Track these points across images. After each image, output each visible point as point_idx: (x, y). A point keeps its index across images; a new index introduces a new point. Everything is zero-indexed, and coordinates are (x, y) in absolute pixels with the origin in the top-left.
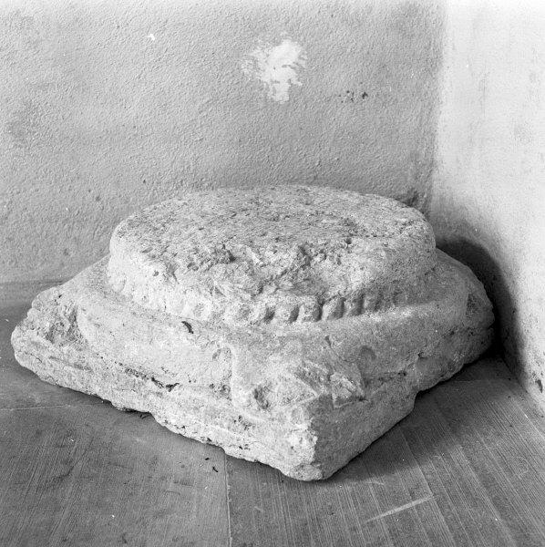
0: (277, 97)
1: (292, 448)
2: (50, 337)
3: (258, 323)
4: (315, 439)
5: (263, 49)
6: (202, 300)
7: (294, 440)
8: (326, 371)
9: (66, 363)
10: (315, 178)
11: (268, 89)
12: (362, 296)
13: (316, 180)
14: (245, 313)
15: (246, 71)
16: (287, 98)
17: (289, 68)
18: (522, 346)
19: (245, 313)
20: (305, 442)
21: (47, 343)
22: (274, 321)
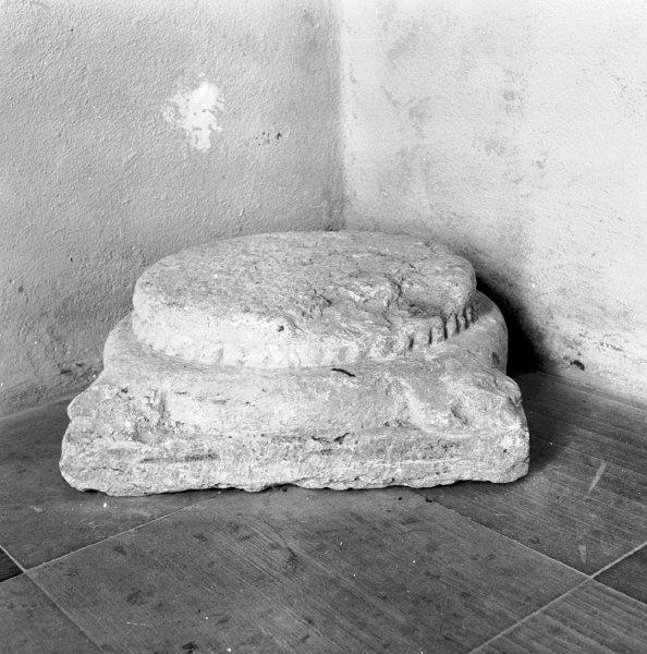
0: (200, 146)
1: (505, 451)
2: (136, 437)
3: (403, 352)
4: (527, 434)
5: (183, 93)
6: (345, 343)
7: (507, 443)
8: (491, 378)
9: (171, 460)
10: (241, 229)
11: (190, 138)
12: (464, 311)
13: (241, 232)
14: (390, 345)
15: (168, 119)
16: (208, 146)
17: (208, 113)
18: (541, 337)
19: (390, 345)
20: (519, 440)
21: (134, 445)
22: (416, 347)
